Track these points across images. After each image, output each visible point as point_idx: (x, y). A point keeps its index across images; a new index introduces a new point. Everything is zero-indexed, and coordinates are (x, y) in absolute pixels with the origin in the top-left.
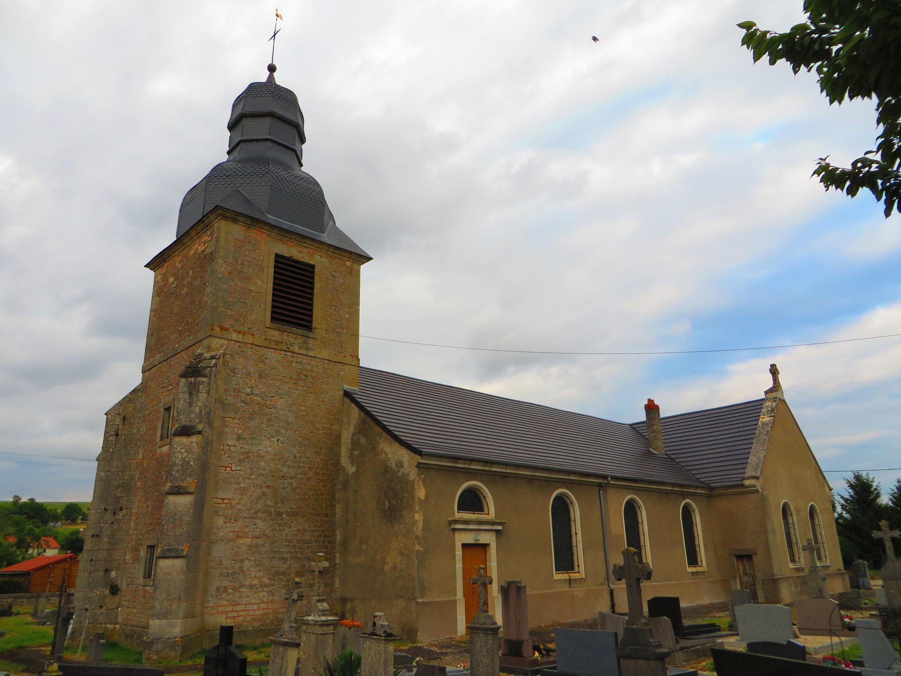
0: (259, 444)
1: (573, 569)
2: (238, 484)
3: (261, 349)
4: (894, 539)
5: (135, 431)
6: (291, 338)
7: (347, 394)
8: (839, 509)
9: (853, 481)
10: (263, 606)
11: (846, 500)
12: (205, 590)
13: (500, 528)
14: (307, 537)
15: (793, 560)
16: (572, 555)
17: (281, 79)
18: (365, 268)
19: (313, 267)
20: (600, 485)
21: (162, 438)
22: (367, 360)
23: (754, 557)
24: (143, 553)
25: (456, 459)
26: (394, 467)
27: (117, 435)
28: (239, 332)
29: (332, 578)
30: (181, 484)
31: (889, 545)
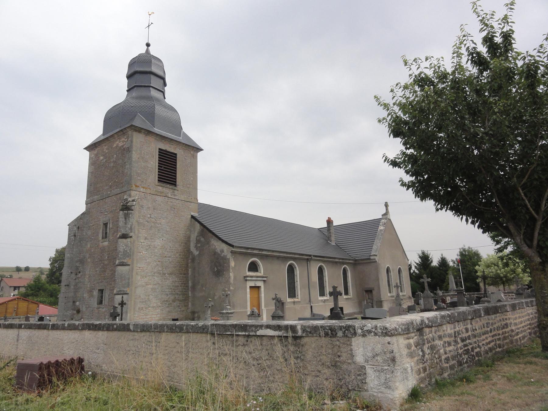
0: (155, 242)
1: (295, 297)
2: (146, 260)
3: (154, 196)
4: (428, 282)
5: (85, 234)
6: (167, 190)
7: (193, 217)
8: (413, 268)
9: (421, 255)
10: (158, 316)
11: (417, 264)
12: (134, 309)
13: (265, 279)
14: (176, 284)
15: (390, 292)
16: (295, 291)
17: (153, 51)
18: (199, 154)
19: (176, 154)
20: (308, 259)
21: (103, 238)
22: (202, 199)
23: (373, 291)
24: (96, 293)
25: (247, 248)
26: (219, 252)
27: (75, 236)
28: (144, 188)
29: (188, 303)
30: (123, 261)
31: (426, 284)
